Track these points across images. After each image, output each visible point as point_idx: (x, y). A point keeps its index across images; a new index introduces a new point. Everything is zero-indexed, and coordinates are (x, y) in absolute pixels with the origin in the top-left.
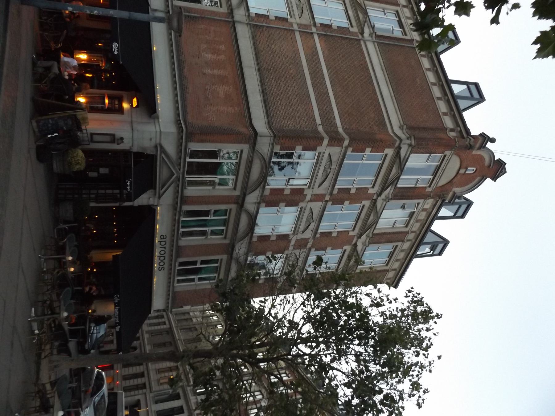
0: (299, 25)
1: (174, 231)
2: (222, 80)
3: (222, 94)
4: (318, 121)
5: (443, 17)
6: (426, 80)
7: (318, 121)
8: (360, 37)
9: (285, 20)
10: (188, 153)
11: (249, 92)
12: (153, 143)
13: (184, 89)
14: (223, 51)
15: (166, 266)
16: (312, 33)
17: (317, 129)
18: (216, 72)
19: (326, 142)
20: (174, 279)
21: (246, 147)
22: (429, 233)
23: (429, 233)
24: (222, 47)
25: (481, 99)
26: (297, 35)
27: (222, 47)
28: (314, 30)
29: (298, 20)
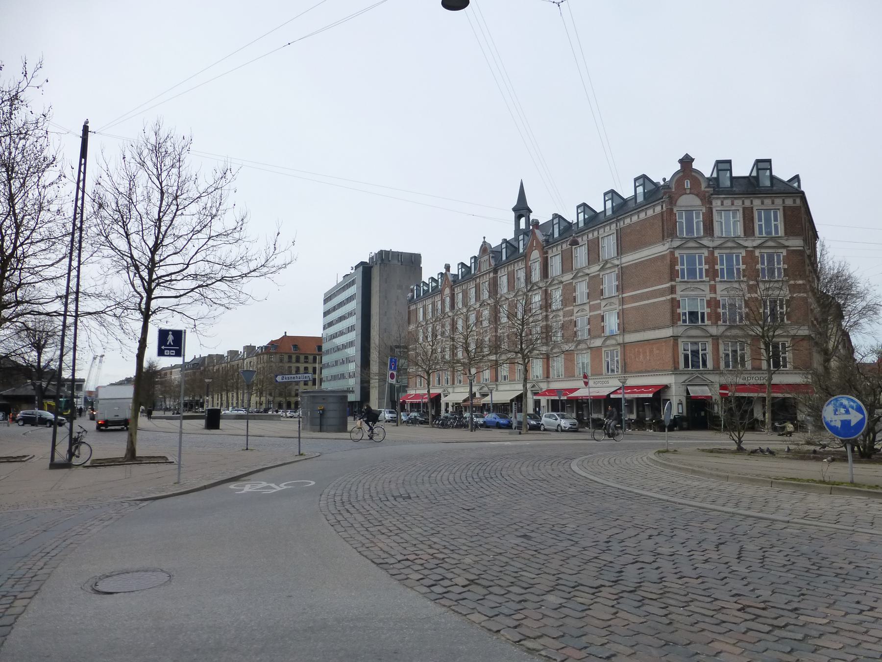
0: (619, 306)
1: (787, 373)
2: (651, 351)
3: (658, 352)
4: (663, 298)
5: (84, 443)
6: (570, 253)
7: (663, 298)
8: (620, 266)
9: (618, 313)
10: (686, 369)
11: (655, 337)
12: (681, 386)
13: (657, 371)
14: (407, 369)
15: (607, 380)
16: (622, 298)
17: (669, 300)
18: (648, 354)
19: (674, 296)
20: (783, 370)
21: (680, 340)
22: (51, 429)
23: (51, 429)
24: (636, 350)
25: (729, 162)
26: (625, 307)
27: (636, 350)
28: (620, 296)
29: (617, 306)
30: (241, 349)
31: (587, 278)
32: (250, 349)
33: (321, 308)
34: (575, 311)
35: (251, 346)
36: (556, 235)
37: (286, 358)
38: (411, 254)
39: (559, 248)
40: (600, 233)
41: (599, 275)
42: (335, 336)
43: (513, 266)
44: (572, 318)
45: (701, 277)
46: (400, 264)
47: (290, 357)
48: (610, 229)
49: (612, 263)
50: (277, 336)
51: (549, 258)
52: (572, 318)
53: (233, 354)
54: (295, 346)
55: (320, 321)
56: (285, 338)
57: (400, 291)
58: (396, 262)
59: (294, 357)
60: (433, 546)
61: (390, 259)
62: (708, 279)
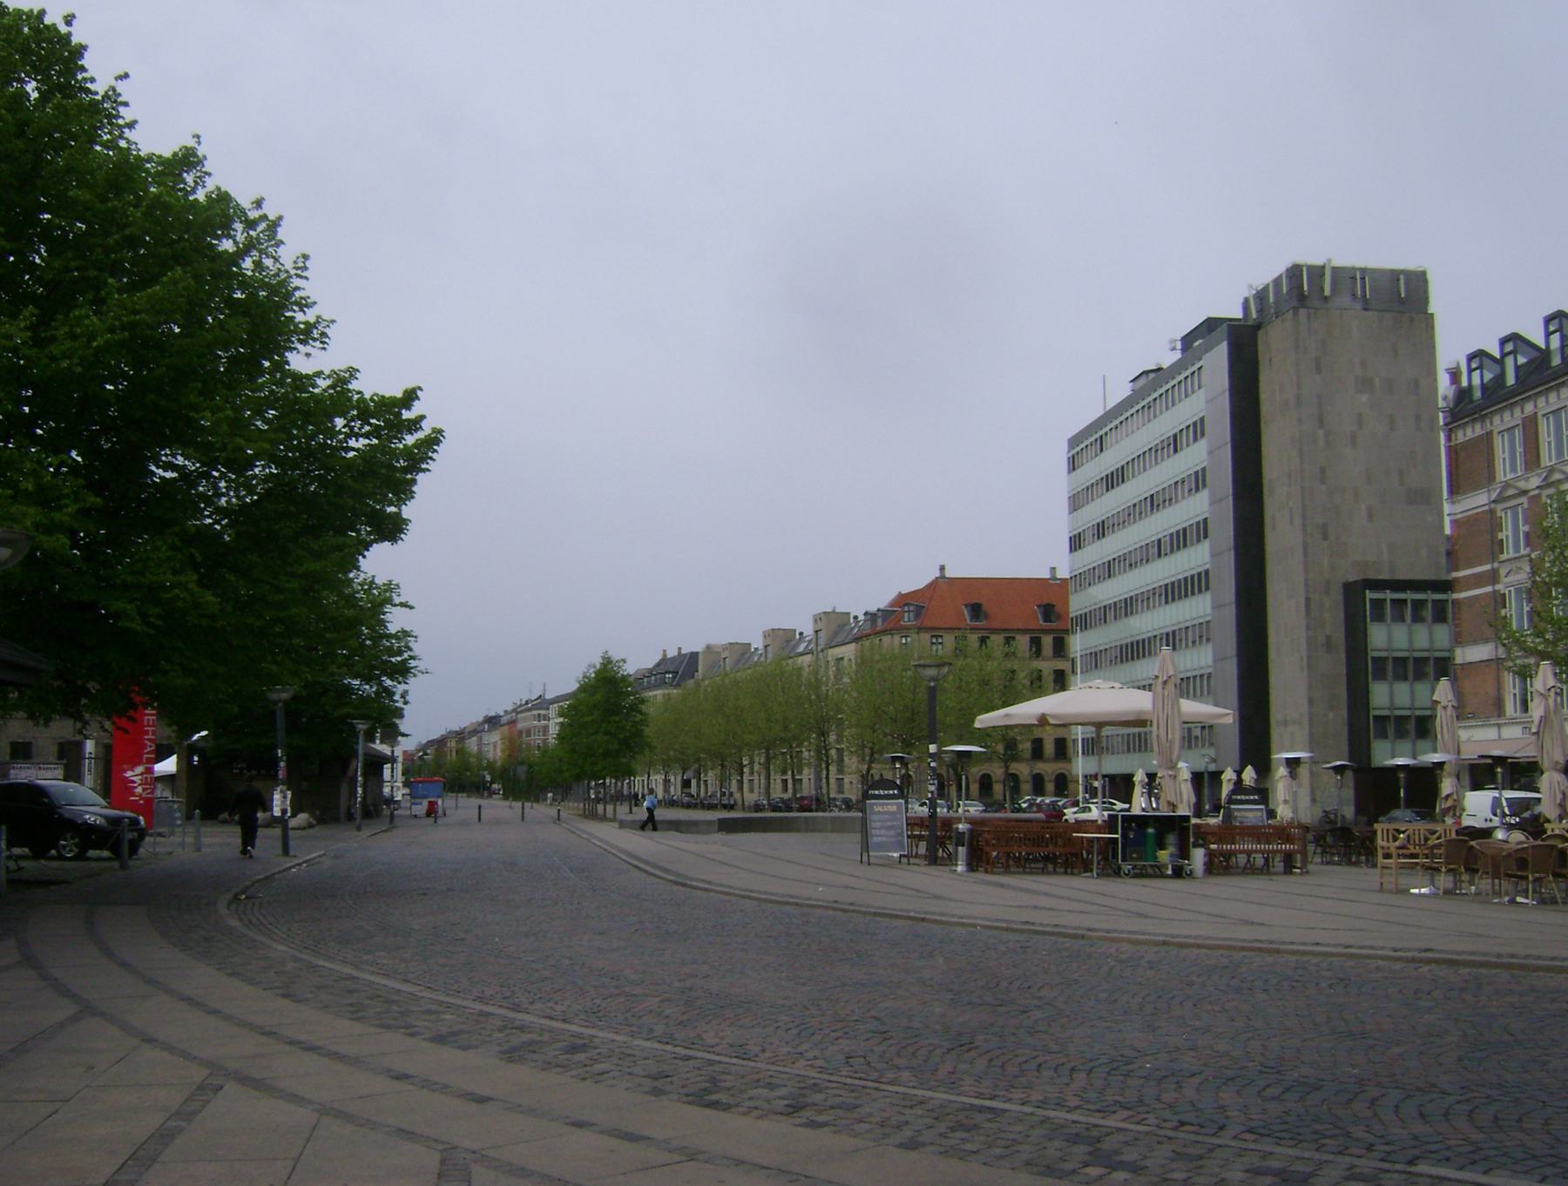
30: (407, 511)
31: (1523, 500)
32: (835, 626)
33: (1060, 484)
34: (1503, 572)
35: (834, 612)
36: (1510, 380)
37: (1023, 642)
38: (1395, 275)
39: (1517, 411)
40: (1495, 424)
41: (1539, 495)
42: (1109, 569)
43: (1488, 421)
44: (1498, 587)
45: (1517, 549)
46: (1358, 306)
47: (1036, 643)
48: (1502, 421)
49: (1516, 488)
50: (917, 579)
51: (1495, 435)
52: (1498, 587)
53: (784, 640)
54: (976, 610)
55: (1061, 526)
56: (942, 586)
57: (1364, 398)
58: (1345, 300)
59: (1047, 641)
60: (1164, 1125)
61: (1327, 292)
62: (1528, 550)
